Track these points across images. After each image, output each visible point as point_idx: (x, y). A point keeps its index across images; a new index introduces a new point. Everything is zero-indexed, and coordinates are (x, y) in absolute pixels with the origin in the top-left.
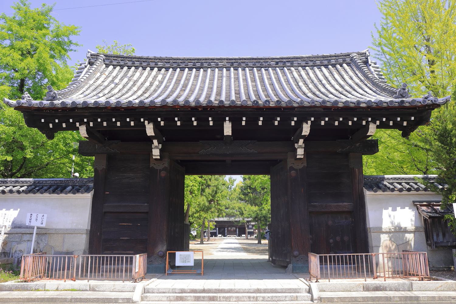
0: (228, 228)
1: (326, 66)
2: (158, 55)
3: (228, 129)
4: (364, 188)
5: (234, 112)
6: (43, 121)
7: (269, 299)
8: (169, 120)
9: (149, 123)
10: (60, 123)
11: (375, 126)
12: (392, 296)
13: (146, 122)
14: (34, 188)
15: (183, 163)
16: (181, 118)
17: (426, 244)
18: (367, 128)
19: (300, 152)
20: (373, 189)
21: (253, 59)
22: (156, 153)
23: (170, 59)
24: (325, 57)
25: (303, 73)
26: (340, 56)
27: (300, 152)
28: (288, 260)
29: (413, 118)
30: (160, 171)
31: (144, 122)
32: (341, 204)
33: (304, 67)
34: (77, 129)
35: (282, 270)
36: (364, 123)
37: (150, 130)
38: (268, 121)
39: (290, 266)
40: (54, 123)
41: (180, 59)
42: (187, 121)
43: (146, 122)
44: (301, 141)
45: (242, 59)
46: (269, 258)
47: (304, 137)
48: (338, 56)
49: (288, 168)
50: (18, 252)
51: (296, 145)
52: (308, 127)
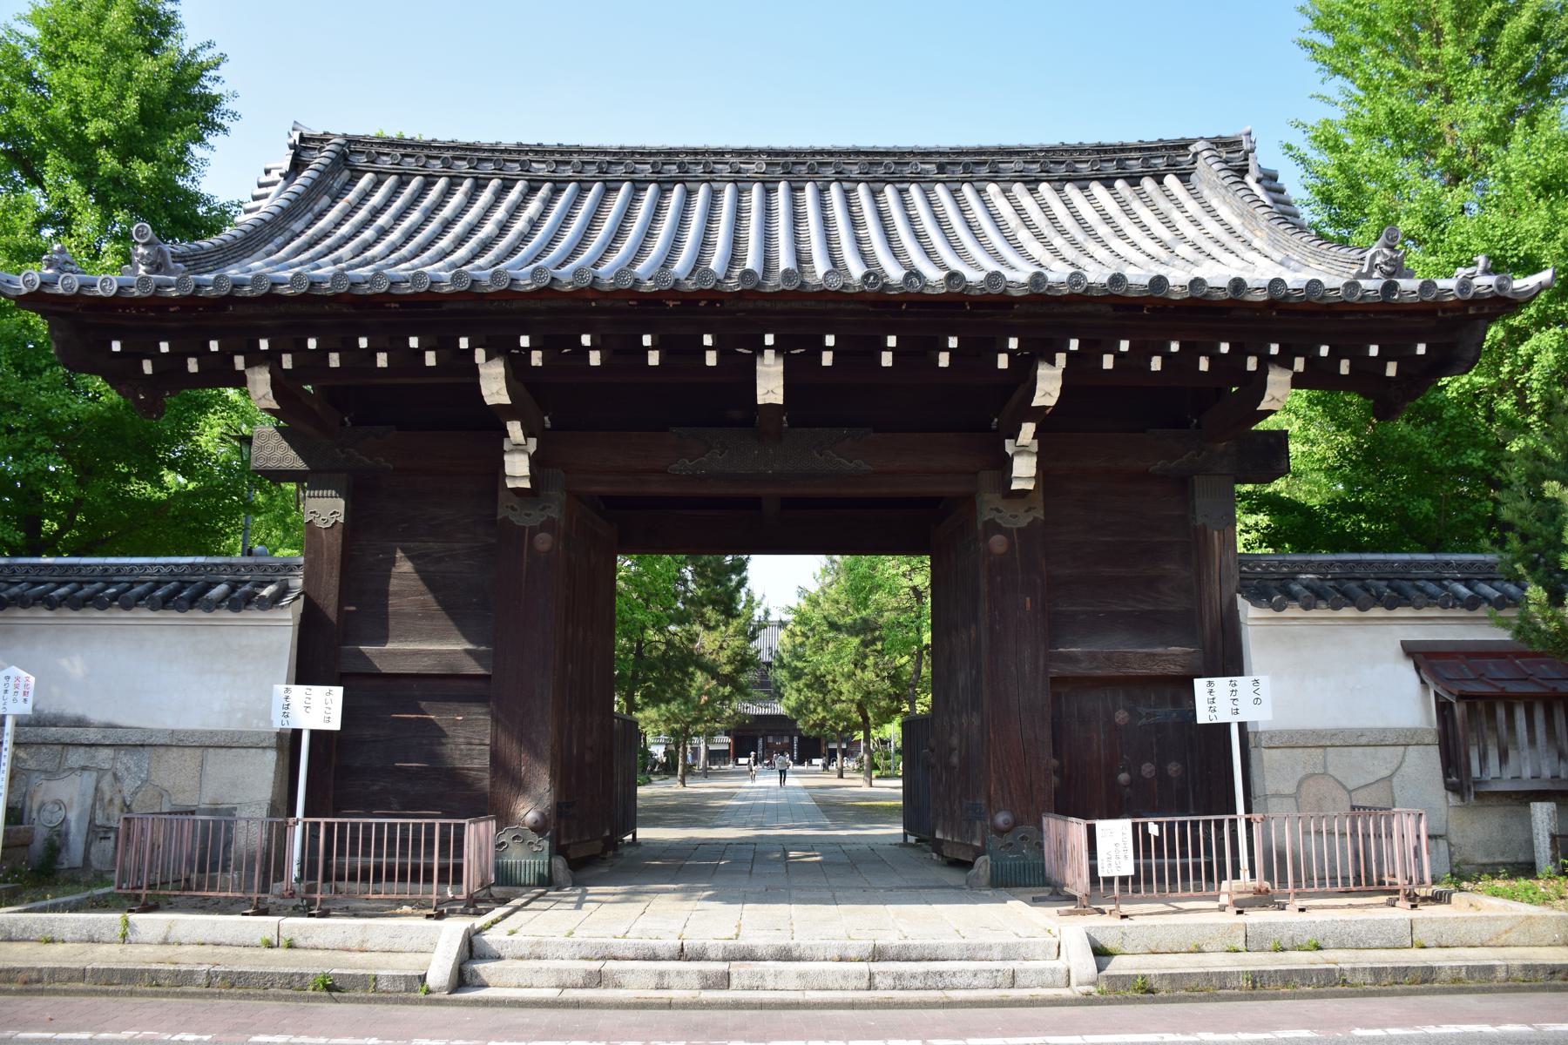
0: (765, 737)
1: (1108, 182)
2: (530, 140)
3: (770, 385)
4: (1239, 596)
5: (796, 313)
6: (116, 346)
7: (918, 984)
8: (558, 341)
9: (488, 359)
10: (178, 357)
11: (1286, 376)
12: (1347, 966)
13: (480, 355)
14: (103, 590)
15: (612, 505)
16: (603, 337)
17: (1442, 786)
18: (1257, 385)
19: (1024, 470)
20: (1270, 600)
21: (858, 153)
22: (517, 468)
23: (571, 153)
24: (1106, 152)
25: (1027, 201)
26: (1156, 149)
27: (1024, 470)
28: (977, 843)
29: (1421, 349)
30: (534, 532)
31: (470, 352)
32: (1159, 650)
33: (1032, 184)
34: (239, 381)
35: (954, 876)
36: (1252, 364)
37: (494, 386)
38: (916, 353)
39: (983, 864)
40: (156, 357)
41: (606, 153)
42: (625, 352)
43: (480, 355)
44: (1028, 429)
45: (821, 152)
46: (905, 835)
47: (1038, 414)
48: (1149, 149)
49: (980, 526)
50: (49, 807)
51: (1009, 447)
52: (1054, 377)
